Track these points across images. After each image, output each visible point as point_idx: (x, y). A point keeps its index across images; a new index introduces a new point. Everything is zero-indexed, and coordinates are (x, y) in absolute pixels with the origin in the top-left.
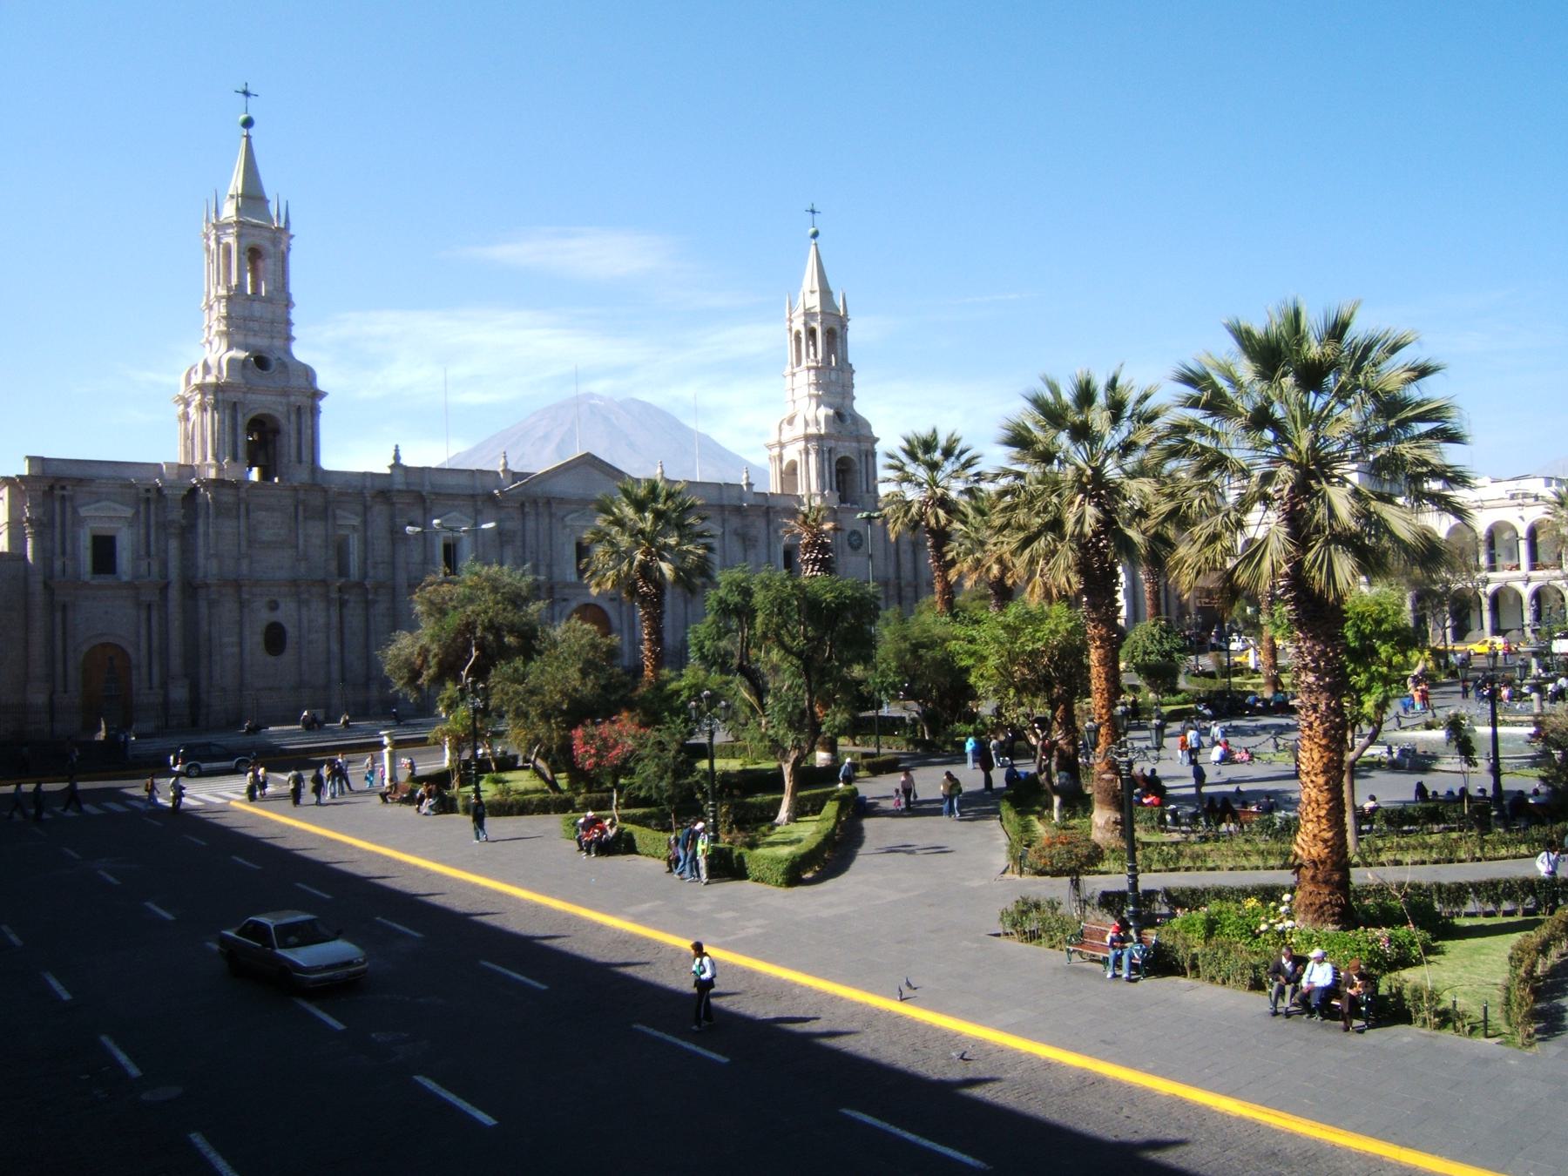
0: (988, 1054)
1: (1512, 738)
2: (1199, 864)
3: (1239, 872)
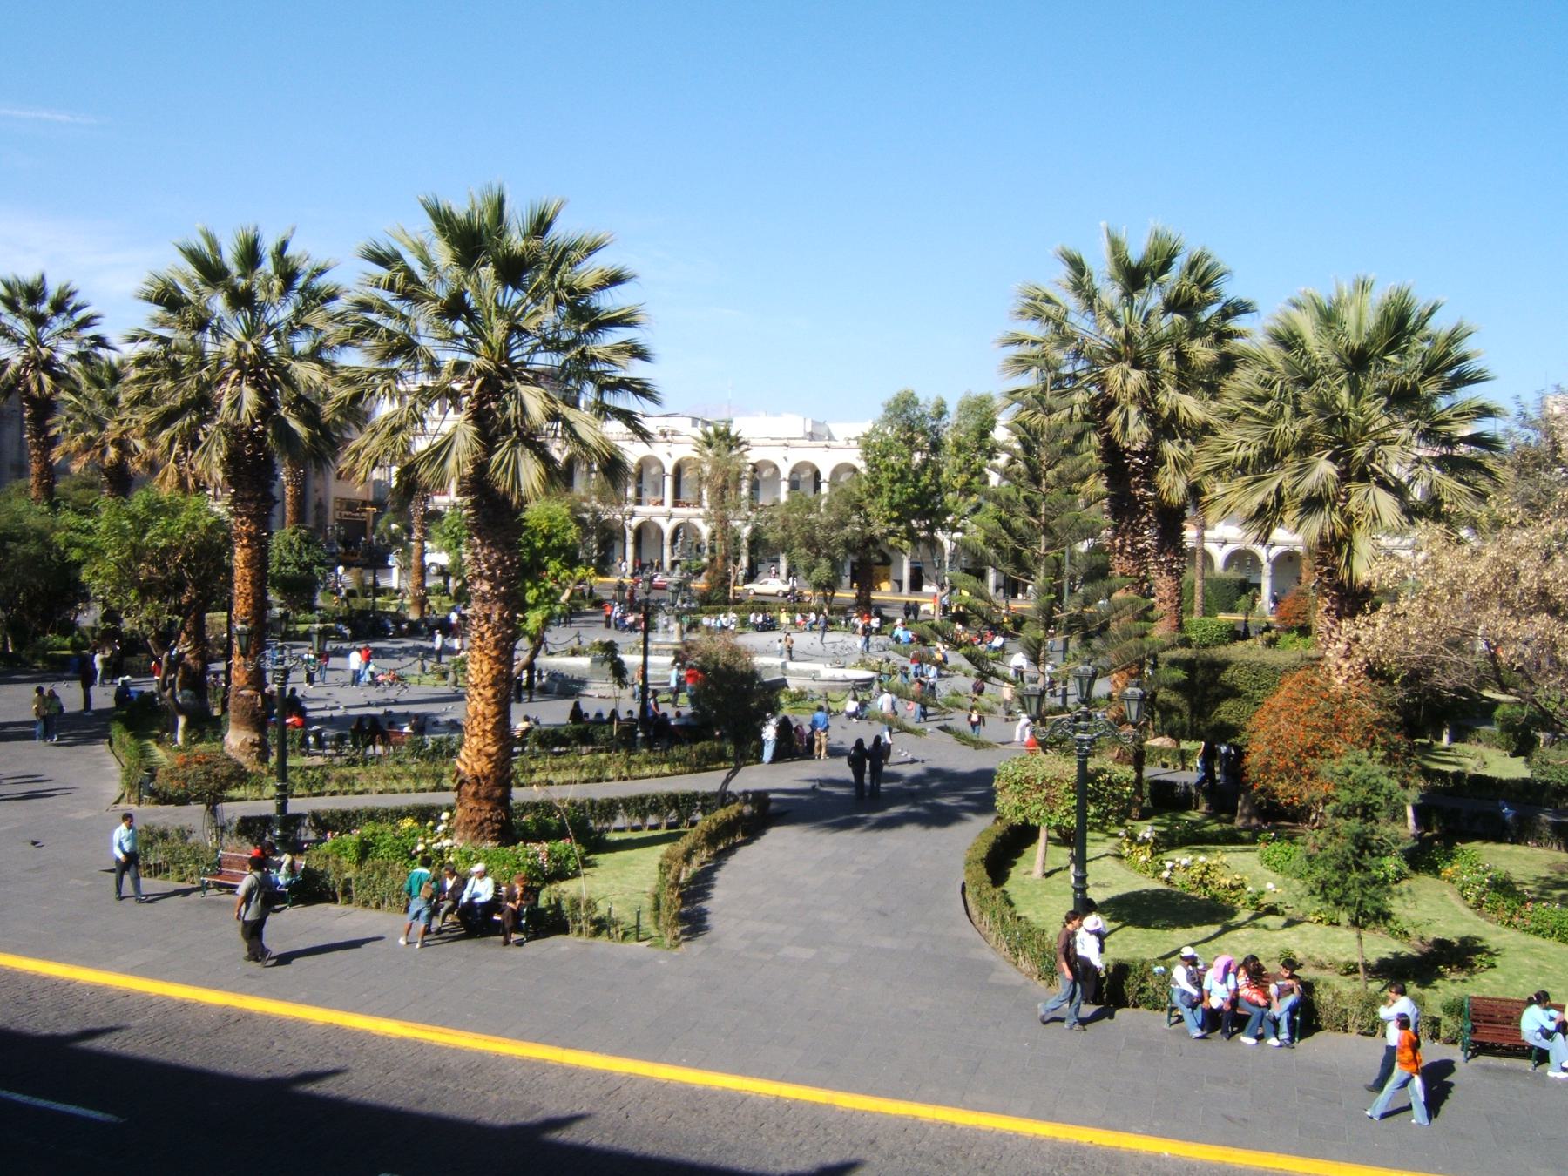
0: (111, 1000)
1: (656, 666)
2: (346, 788)
3: (389, 796)
